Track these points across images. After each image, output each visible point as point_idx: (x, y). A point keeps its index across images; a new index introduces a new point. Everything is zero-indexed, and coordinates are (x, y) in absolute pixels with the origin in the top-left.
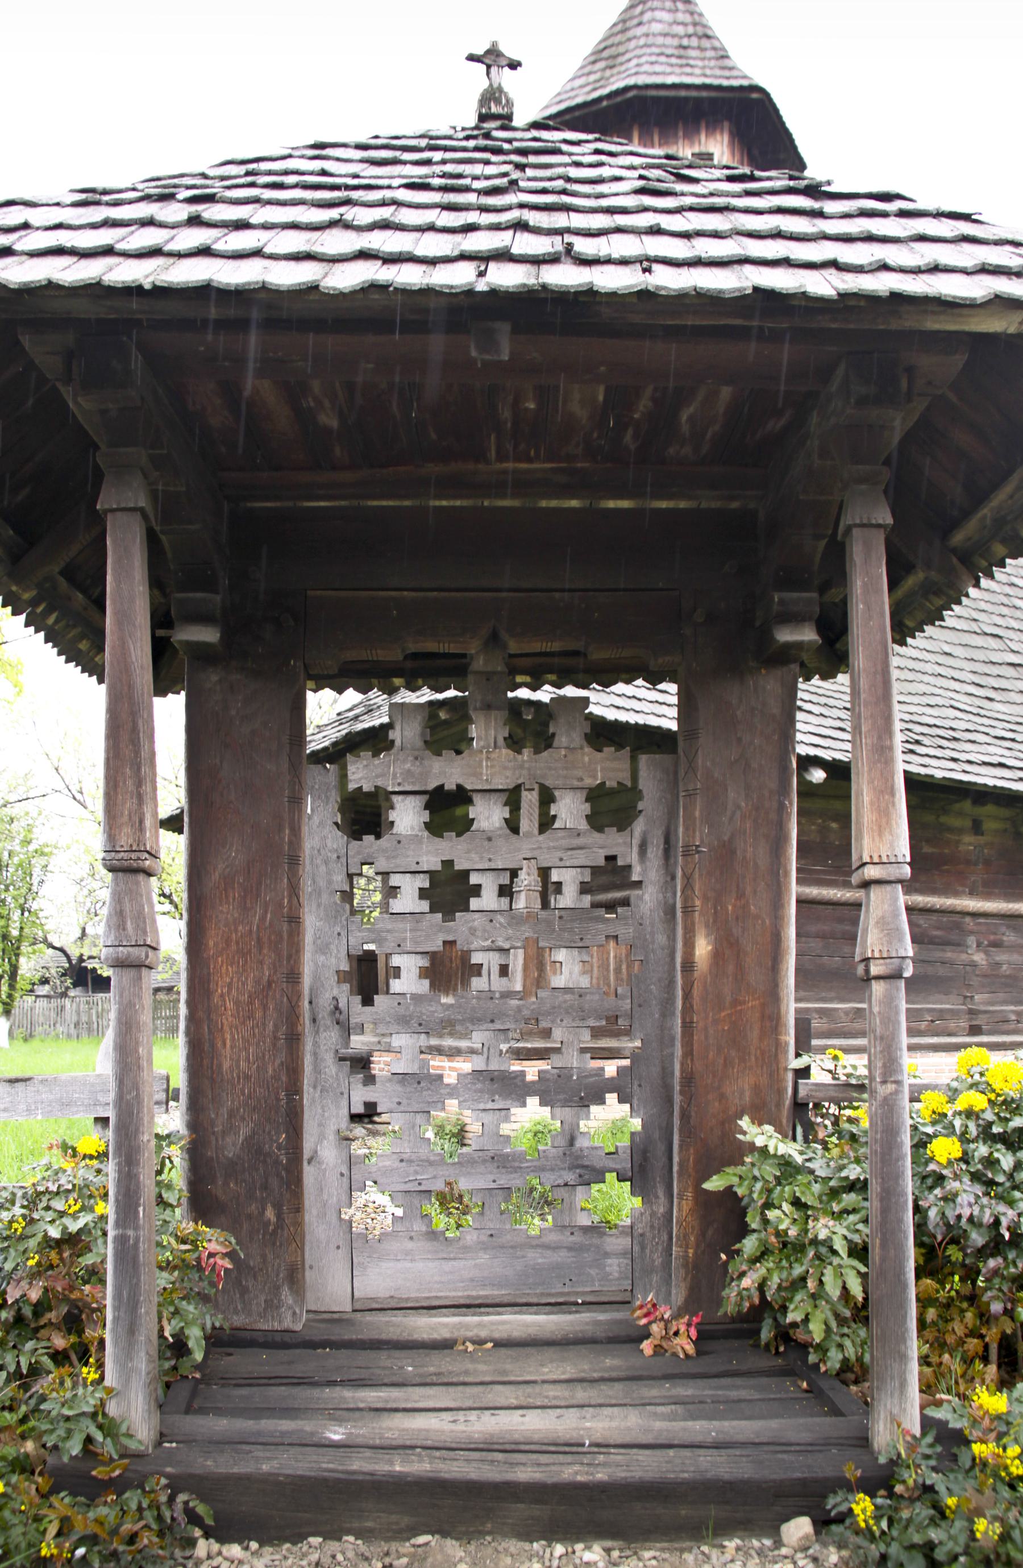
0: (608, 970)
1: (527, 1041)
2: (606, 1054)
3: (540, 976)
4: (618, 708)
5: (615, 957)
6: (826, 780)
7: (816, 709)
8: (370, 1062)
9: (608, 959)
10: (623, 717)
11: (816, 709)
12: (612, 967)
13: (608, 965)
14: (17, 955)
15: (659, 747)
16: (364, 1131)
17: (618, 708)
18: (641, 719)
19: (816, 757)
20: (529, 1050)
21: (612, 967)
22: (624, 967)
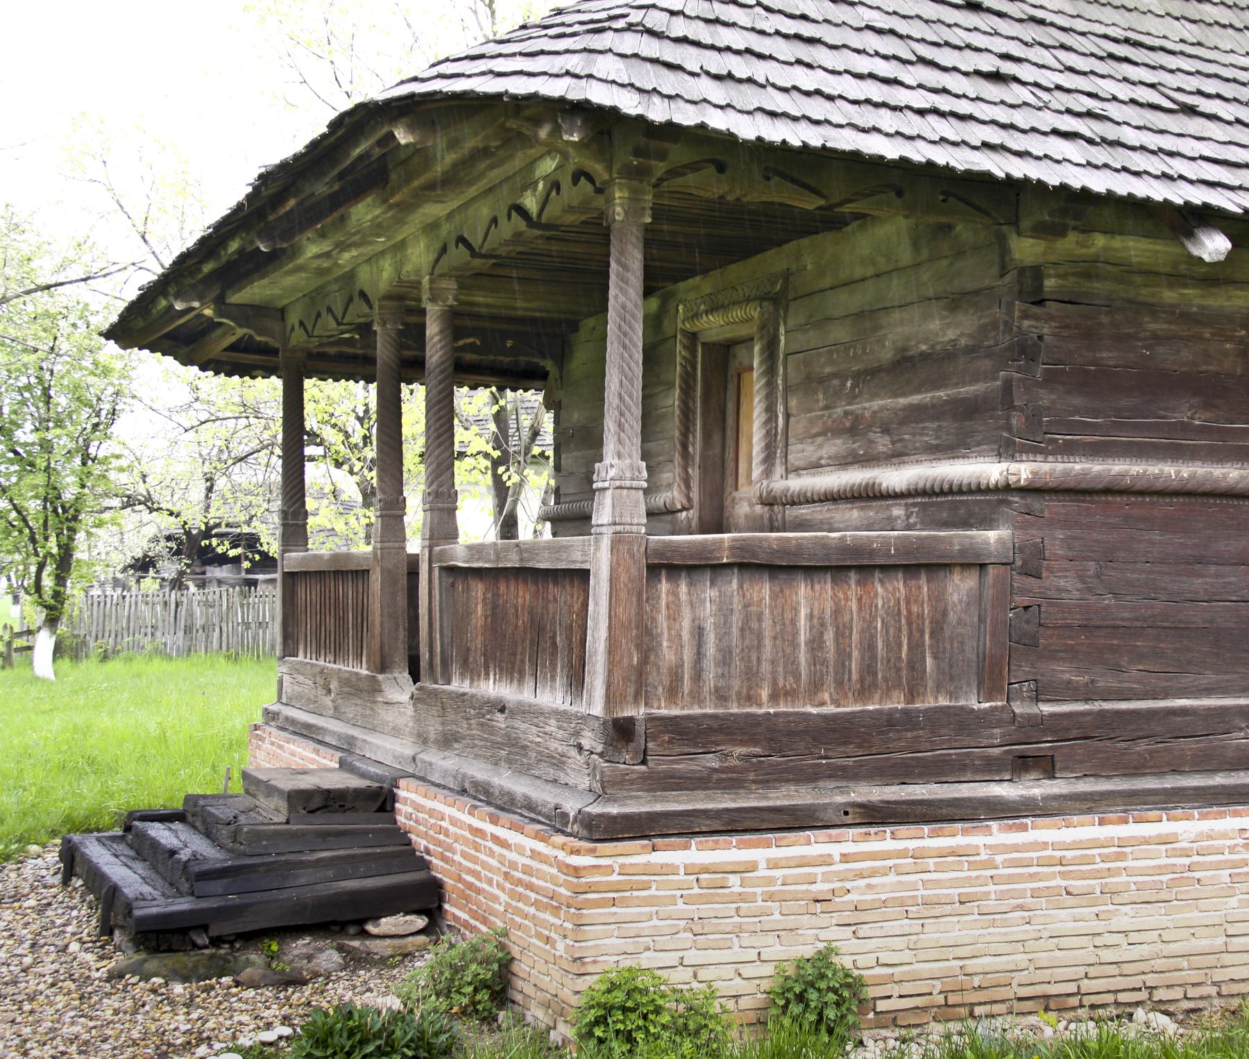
0: (794, 645)
1: (613, 800)
2: (786, 820)
3: (645, 661)
4: (773, 114)
5: (811, 617)
6: (1230, 254)
7: (1227, 111)
8: (393, 798)
9: (794, 622)
10: (775, 132)
11: (1227, 111)
12: (802, 638)
13: (795, 634)
14: (73, 530)
15: (900, 194)
16: (336, 957)
17: (773, 114)
18: (815, 137)
19: (1206, 206)
20: (612, 819)
21: (802, 638)
22: (829, 636)
